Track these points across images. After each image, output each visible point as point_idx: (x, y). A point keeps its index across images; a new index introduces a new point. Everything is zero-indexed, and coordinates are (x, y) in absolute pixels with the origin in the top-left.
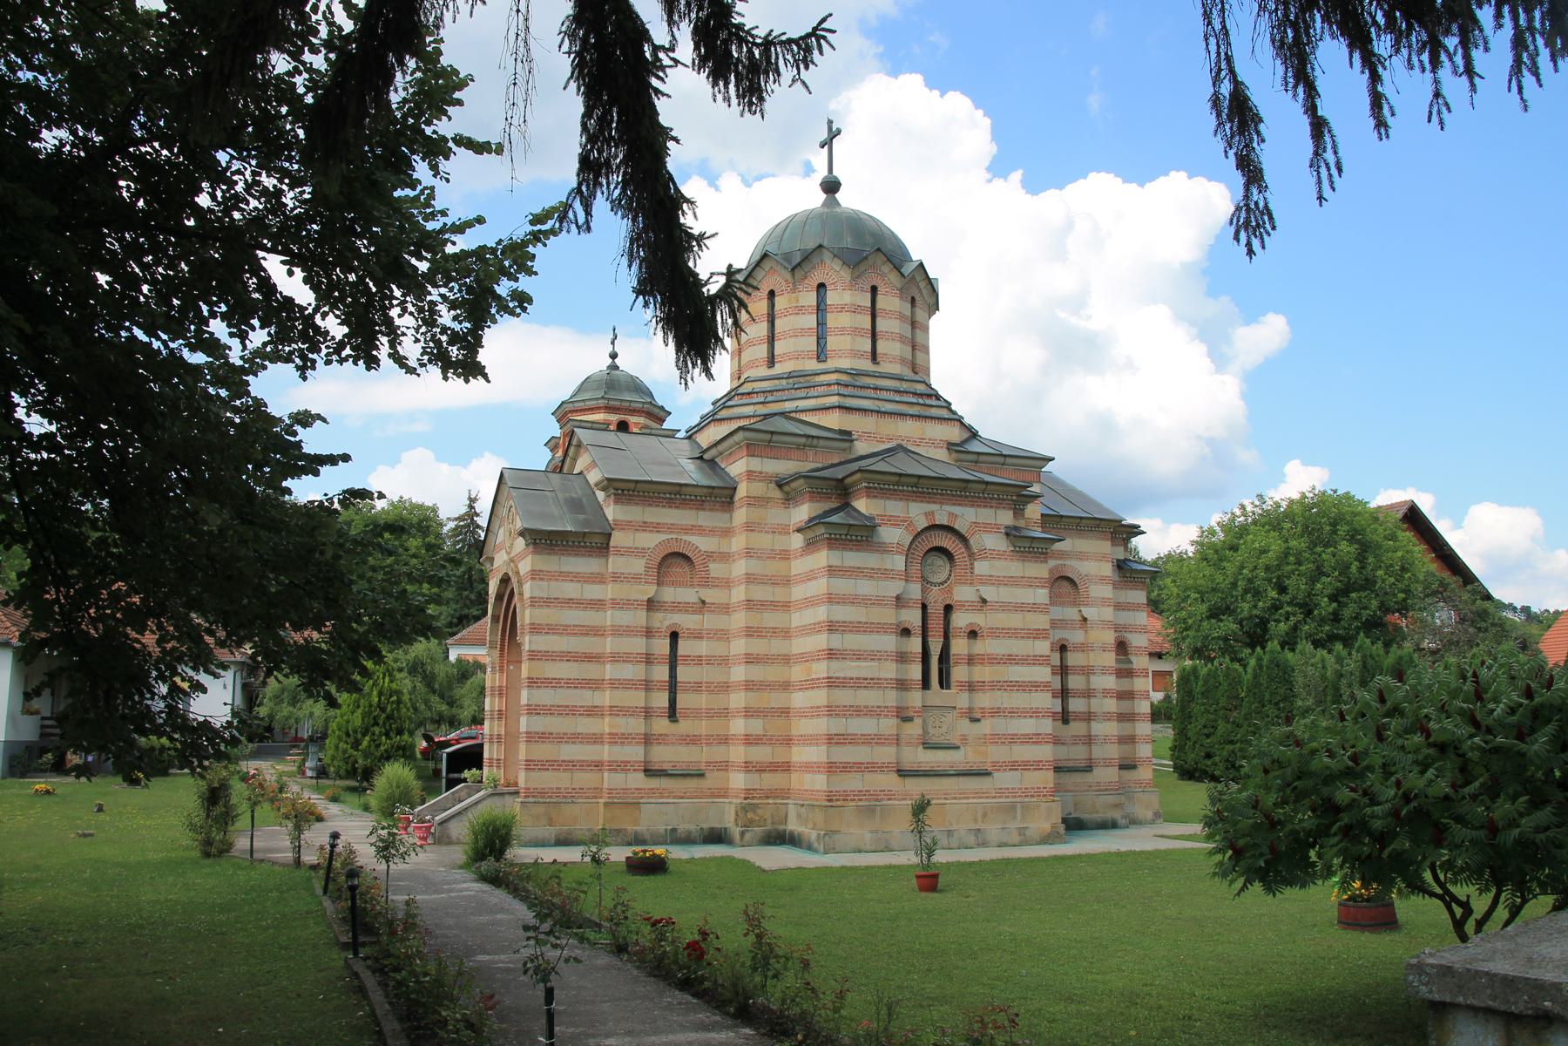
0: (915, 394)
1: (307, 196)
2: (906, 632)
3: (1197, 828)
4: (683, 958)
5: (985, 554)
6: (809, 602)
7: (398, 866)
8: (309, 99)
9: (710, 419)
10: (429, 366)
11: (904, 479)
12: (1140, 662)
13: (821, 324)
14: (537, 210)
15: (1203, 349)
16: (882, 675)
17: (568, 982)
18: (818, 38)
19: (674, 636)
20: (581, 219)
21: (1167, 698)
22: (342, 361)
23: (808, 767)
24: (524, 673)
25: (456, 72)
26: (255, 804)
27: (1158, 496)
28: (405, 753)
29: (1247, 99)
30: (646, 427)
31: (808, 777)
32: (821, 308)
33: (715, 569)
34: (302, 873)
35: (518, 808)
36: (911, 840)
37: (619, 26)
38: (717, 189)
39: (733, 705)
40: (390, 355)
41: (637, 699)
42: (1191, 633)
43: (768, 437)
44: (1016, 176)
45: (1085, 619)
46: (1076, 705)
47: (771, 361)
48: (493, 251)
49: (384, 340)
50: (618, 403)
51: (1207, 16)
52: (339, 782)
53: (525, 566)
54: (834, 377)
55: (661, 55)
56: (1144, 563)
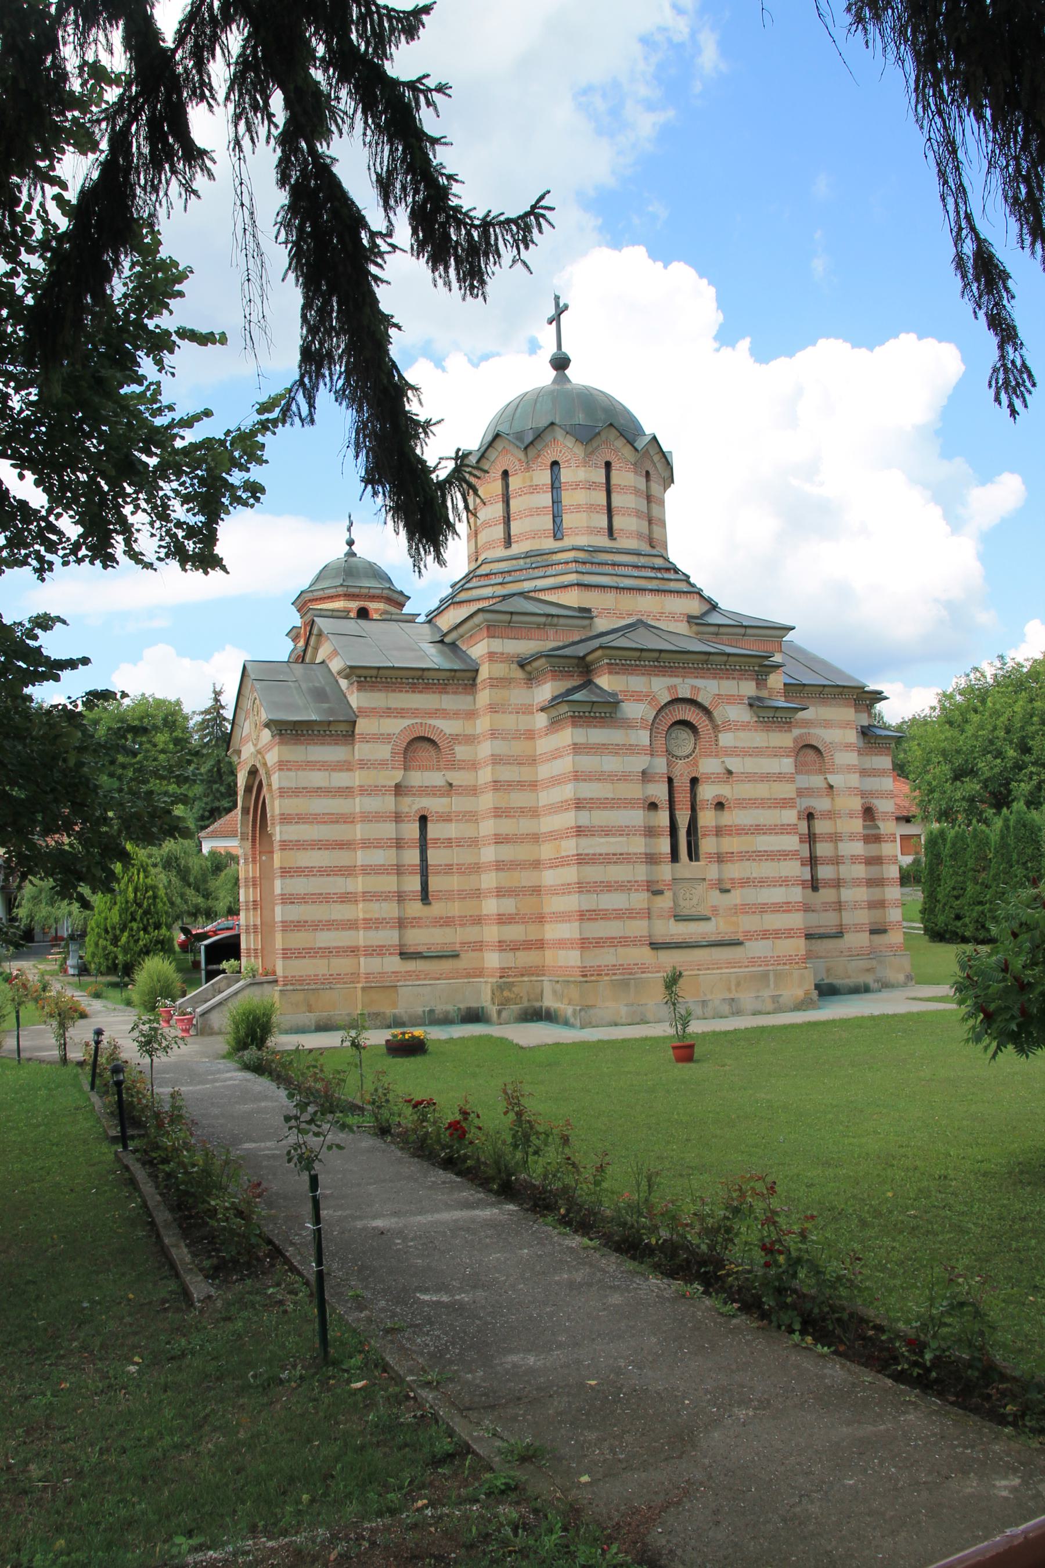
0: (653, 568)
1: (33, 398)
2: (653, 806)
3: (946, 990)
4: (445, 1137)
5: (730, 726)
6: (556, 781)
7: (161, 1059)
8: (29, 300)
9: (450, 602)
10: (167, 561)
11: (644, 654)
12: (888, 827)
13: (556, 502)
14: (264, 399)
15: (937, 512)
16: (632, 850)
17: (332, 1171)
18: (537, 217)
19: (423, 820)
20: (305, 410)
21: (916, 862)
22: (79, 561)
23: (562, 944)
24: (277, 864)
25: (175, 264)
26: (19, 1004)
27: (898, 660)
28: (164, 946)
29: (991, 256)
30: (386, 612)
31: (562, 953)
32: (555, 486)
33: (461, 751)
34: (71, 1069)
35: (277, 995)
36: (665, 1011)
37: (335, 213)
38: (444, 370)
39: (484, 886)
40: (125, 552)
41: (389, 883)
42: (936, 795)
43: (507, 617)
44: (745, 344)
45: (831, 787)
46: (825, 872)
47: (508, 541)
48: (222, 443)
49: (120, 538)
50: (356, 591)
51: (942, 174)
52: (101, 979)
53: (272, 757)
54: (571, 555)
55: (379, 241)
56: (887, 728)
